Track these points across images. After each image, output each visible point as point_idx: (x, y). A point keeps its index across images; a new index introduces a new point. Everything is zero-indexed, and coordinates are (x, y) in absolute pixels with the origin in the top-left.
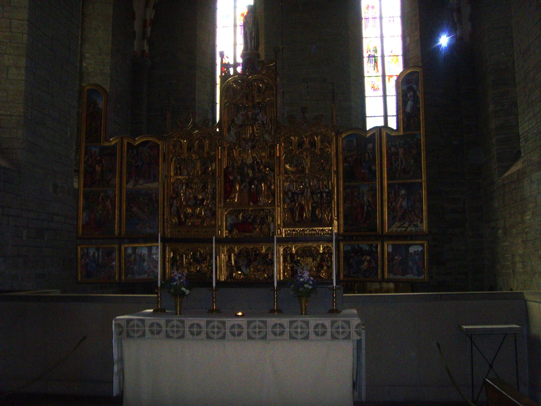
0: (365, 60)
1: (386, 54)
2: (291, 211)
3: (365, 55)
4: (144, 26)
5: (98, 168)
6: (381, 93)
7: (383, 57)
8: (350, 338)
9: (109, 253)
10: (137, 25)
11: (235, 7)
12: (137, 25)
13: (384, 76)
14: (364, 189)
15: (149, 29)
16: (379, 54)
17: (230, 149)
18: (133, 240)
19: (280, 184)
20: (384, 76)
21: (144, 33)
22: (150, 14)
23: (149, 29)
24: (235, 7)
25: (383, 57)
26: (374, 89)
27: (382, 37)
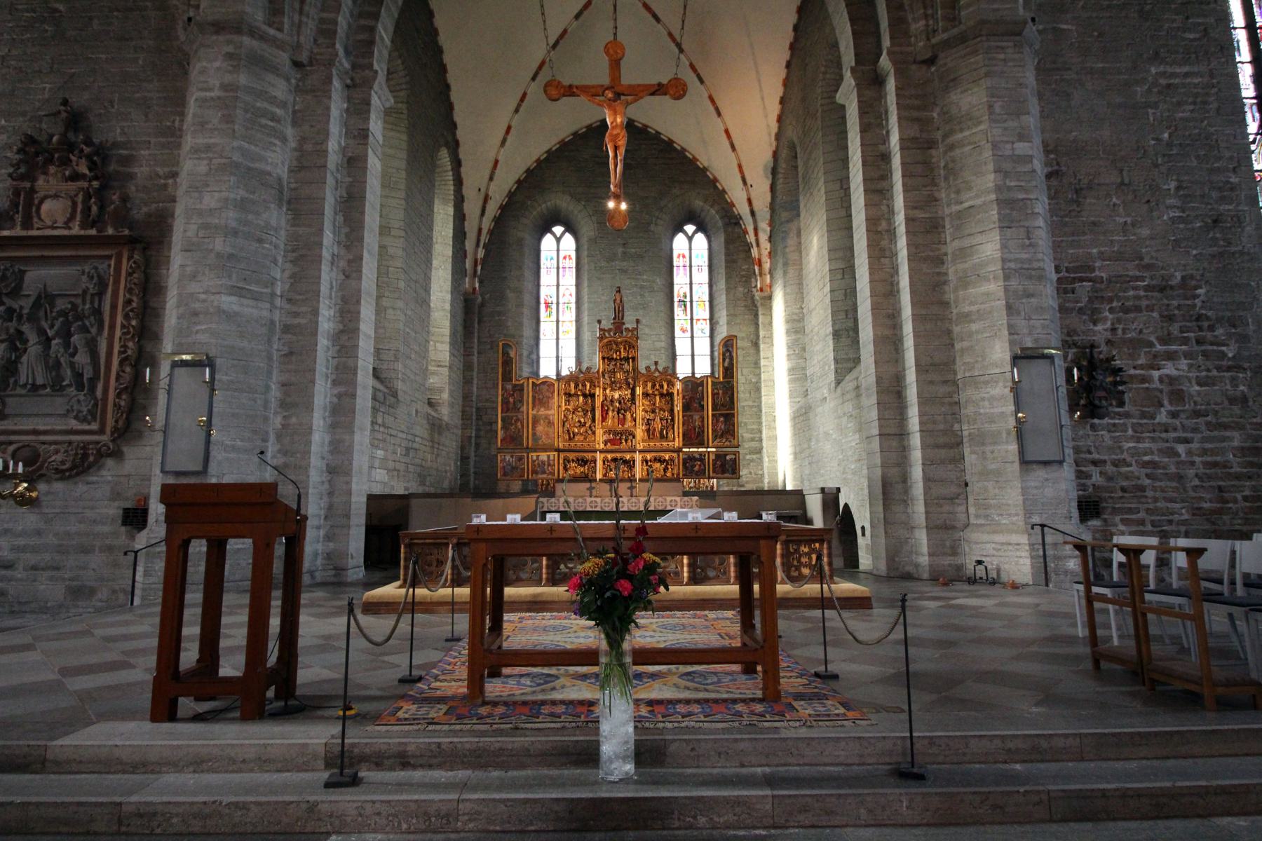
0: (676, 304)
1: (695, 299)
2: (648, 431)
3: (676, 299)
4: (476, 265)
5: (511, 400)
6: (689, 334)
7: (691, 302)
8: (591, 704)
9: (520, 459)
10: (468, 264)
11: (558, 250)
12: (468, 264)
13: (692, 319)
14: (696, 417)
15: (479, 268)
16: (688, 299)
17: (605, 389)
18: (535, 450)
19: (640, 414)
20: (692, 319)
21: (475, 271)
22: (481, 253)
23: (479, 268)
24: (558, 250)
25: (691, 302)
26: (683, 331)
27: (691, 284)
